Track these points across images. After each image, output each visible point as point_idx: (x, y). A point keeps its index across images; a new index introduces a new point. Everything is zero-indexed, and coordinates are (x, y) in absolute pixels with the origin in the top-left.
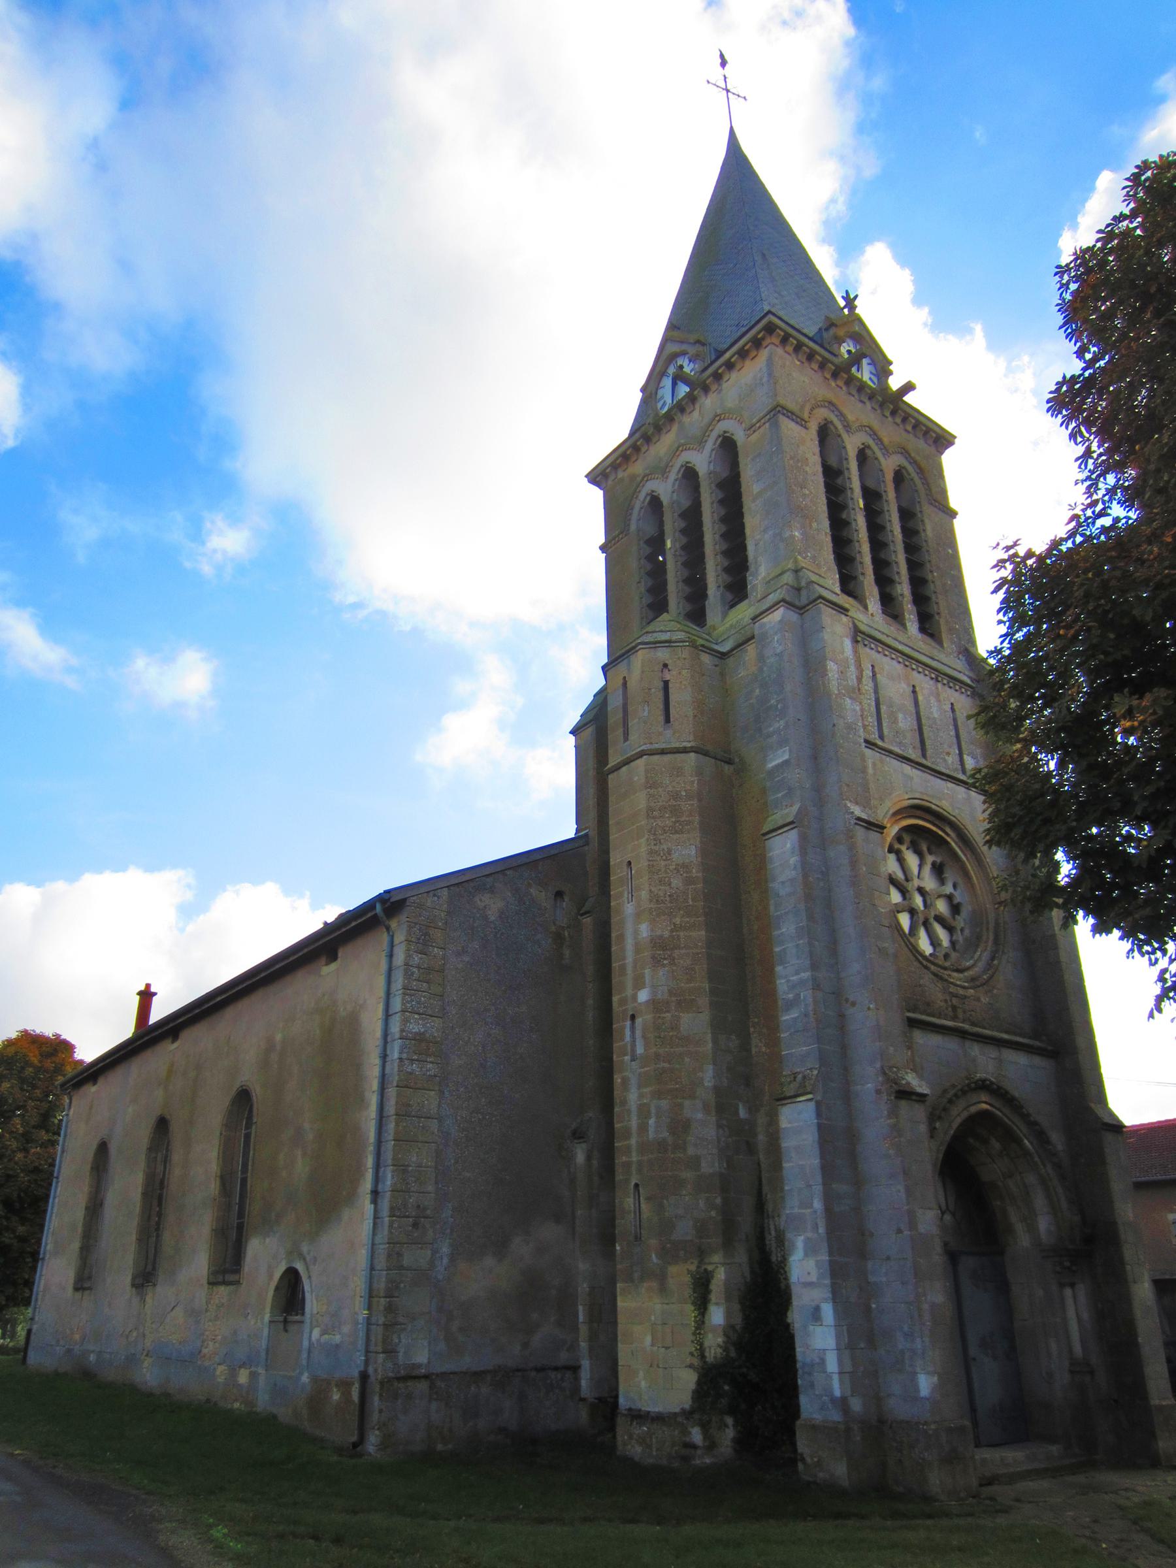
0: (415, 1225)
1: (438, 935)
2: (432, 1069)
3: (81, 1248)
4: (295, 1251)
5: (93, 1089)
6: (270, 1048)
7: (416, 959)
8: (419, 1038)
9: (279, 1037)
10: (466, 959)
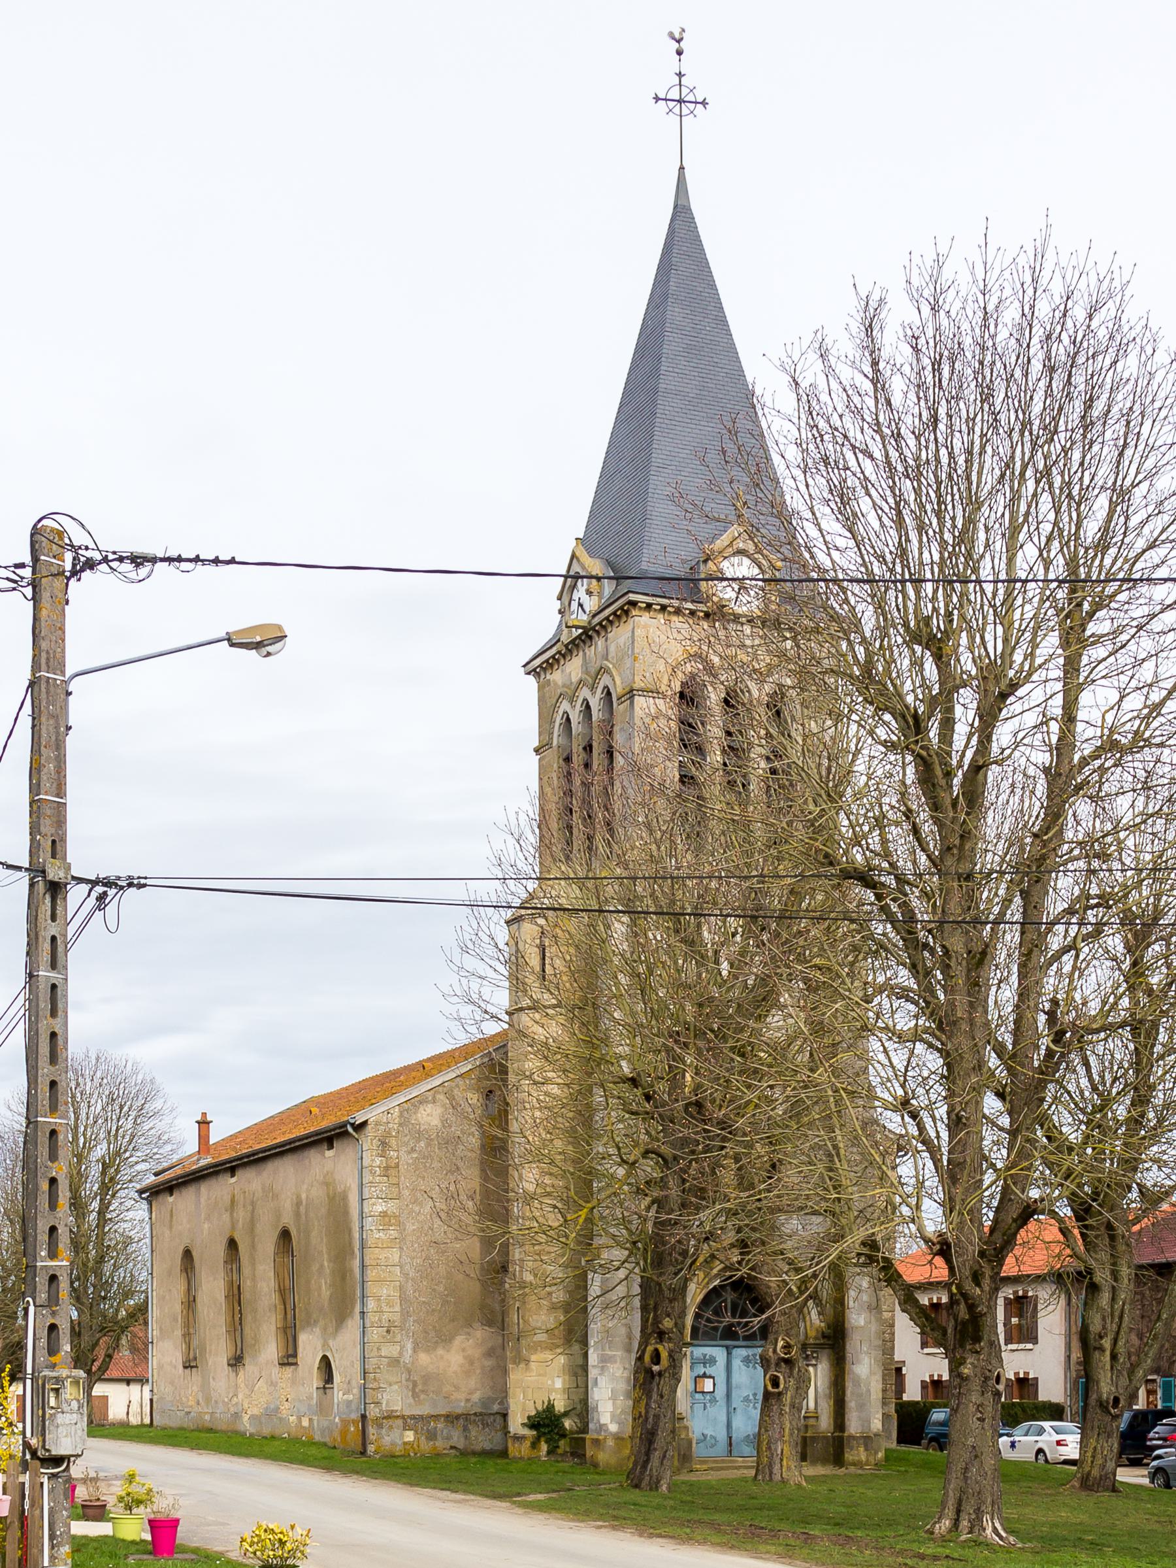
0: (388, 1331)
1: (393, 1142)
2: (394, 1234)
3: (184, 1336)
4: (325, 1345)
5: (171, 1199)
6: (299, 1204)
7: (378, 1161)
8: (384, 1214)
9: (304, 1196)
10: (415, 1155)
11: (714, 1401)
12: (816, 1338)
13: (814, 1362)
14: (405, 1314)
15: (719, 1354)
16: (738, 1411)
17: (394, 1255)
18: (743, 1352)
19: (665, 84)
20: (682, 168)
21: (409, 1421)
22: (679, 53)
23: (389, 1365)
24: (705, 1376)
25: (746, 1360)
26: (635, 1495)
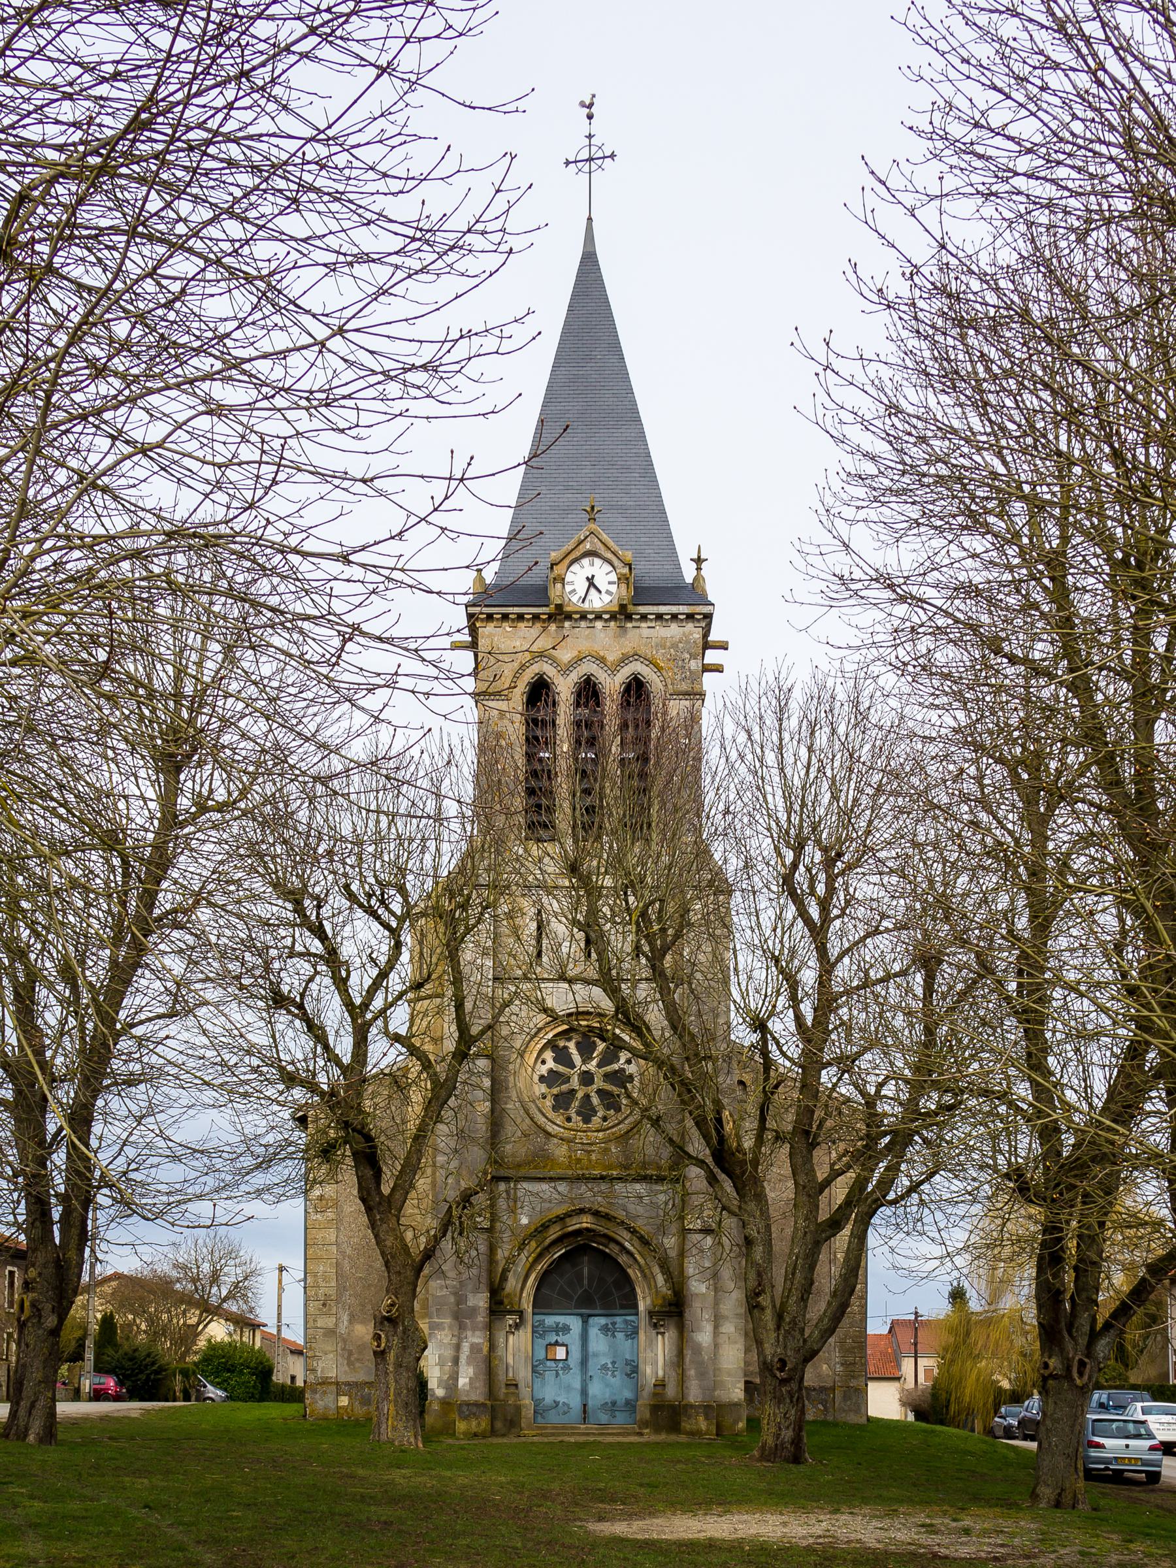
0: (324, 1305)
11: (567, 1368)
14: (341, 1289)
15: (574, 1323)
16: (595, 1379)
17: (331, 1236)
18: (603, 1321)
19: (575, 146)
20: (590, 219)
21: (340, 1387)
22: (590, 117)
23: (325, 1335)
24: (557, 1344)
25: (605, 1329)
26: (1058, 1513)
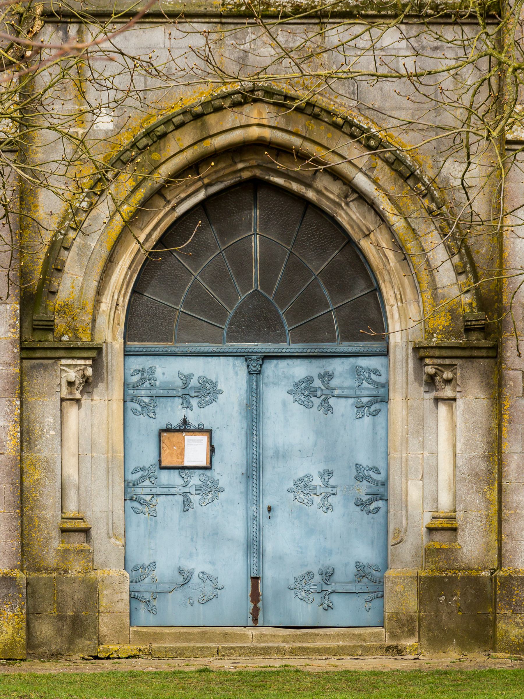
11: (211, 489)
12: (447, 332)
13: (448, 392)
15: (229, 375)
16: (280, 515)
24: (184, 427)
